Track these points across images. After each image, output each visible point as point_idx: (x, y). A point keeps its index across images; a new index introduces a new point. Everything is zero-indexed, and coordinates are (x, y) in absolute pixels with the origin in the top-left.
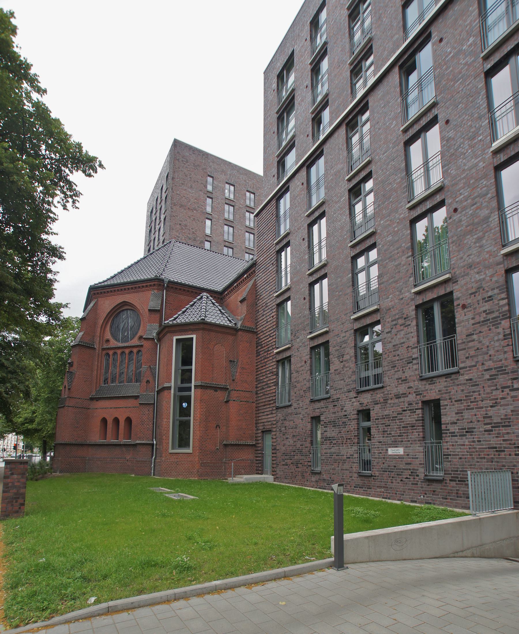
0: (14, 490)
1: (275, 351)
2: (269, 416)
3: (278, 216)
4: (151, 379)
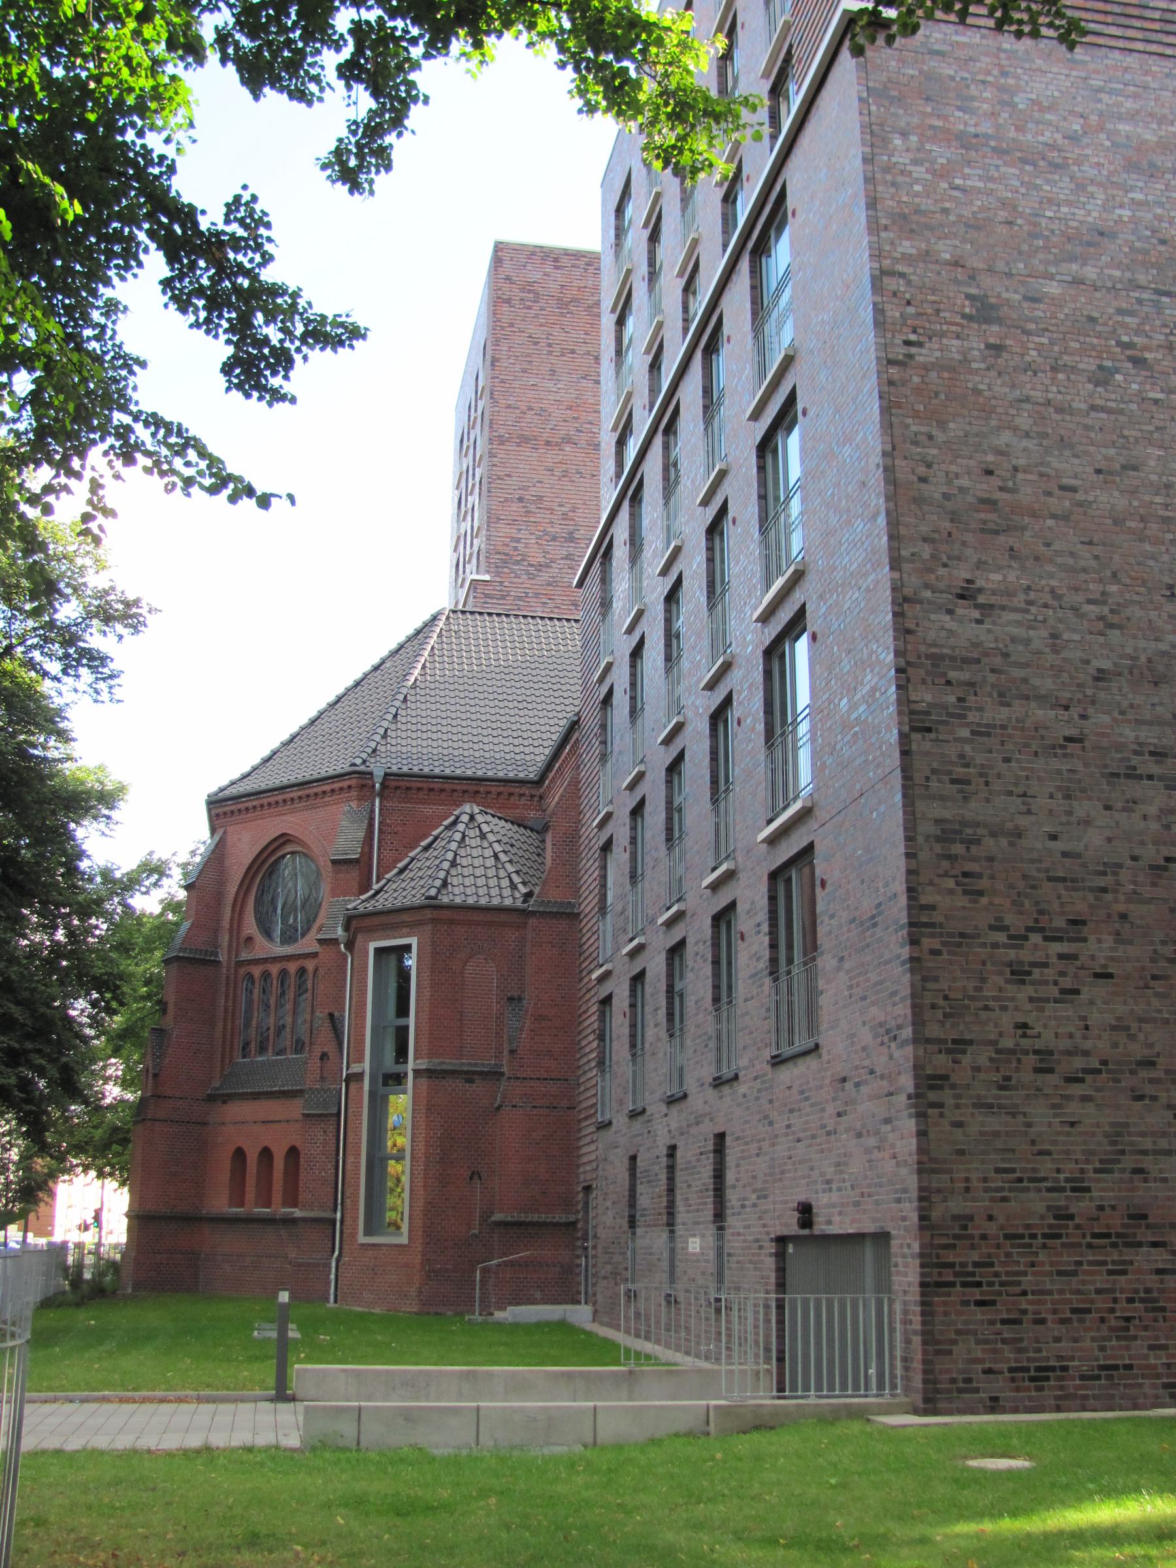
1: (594, 976)
4: (331, 1049)
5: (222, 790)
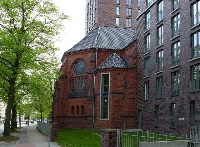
0: (55, 132)
2: (141, 104)
3: (145, 21)
4: (92, 90)
5: (67, 51)
